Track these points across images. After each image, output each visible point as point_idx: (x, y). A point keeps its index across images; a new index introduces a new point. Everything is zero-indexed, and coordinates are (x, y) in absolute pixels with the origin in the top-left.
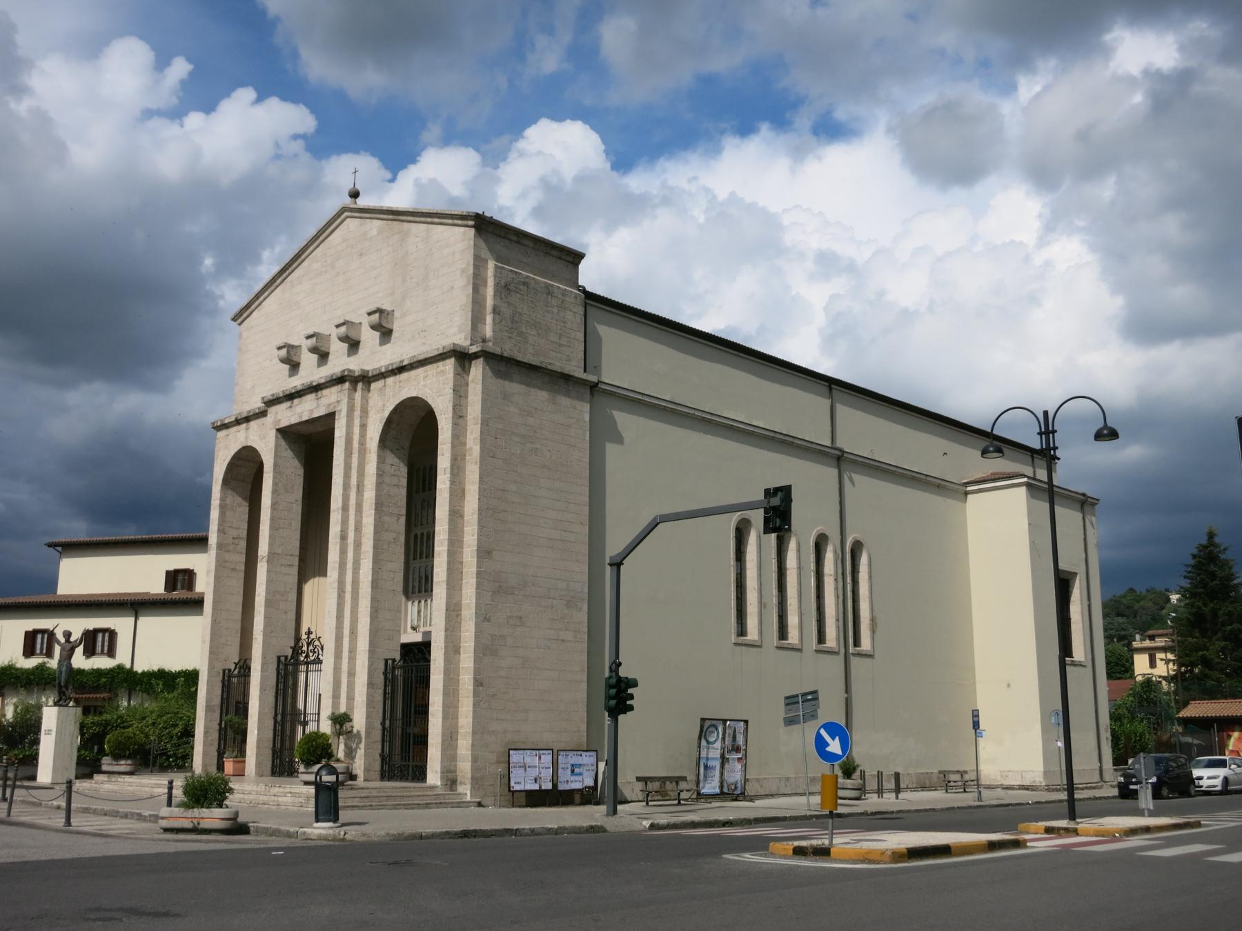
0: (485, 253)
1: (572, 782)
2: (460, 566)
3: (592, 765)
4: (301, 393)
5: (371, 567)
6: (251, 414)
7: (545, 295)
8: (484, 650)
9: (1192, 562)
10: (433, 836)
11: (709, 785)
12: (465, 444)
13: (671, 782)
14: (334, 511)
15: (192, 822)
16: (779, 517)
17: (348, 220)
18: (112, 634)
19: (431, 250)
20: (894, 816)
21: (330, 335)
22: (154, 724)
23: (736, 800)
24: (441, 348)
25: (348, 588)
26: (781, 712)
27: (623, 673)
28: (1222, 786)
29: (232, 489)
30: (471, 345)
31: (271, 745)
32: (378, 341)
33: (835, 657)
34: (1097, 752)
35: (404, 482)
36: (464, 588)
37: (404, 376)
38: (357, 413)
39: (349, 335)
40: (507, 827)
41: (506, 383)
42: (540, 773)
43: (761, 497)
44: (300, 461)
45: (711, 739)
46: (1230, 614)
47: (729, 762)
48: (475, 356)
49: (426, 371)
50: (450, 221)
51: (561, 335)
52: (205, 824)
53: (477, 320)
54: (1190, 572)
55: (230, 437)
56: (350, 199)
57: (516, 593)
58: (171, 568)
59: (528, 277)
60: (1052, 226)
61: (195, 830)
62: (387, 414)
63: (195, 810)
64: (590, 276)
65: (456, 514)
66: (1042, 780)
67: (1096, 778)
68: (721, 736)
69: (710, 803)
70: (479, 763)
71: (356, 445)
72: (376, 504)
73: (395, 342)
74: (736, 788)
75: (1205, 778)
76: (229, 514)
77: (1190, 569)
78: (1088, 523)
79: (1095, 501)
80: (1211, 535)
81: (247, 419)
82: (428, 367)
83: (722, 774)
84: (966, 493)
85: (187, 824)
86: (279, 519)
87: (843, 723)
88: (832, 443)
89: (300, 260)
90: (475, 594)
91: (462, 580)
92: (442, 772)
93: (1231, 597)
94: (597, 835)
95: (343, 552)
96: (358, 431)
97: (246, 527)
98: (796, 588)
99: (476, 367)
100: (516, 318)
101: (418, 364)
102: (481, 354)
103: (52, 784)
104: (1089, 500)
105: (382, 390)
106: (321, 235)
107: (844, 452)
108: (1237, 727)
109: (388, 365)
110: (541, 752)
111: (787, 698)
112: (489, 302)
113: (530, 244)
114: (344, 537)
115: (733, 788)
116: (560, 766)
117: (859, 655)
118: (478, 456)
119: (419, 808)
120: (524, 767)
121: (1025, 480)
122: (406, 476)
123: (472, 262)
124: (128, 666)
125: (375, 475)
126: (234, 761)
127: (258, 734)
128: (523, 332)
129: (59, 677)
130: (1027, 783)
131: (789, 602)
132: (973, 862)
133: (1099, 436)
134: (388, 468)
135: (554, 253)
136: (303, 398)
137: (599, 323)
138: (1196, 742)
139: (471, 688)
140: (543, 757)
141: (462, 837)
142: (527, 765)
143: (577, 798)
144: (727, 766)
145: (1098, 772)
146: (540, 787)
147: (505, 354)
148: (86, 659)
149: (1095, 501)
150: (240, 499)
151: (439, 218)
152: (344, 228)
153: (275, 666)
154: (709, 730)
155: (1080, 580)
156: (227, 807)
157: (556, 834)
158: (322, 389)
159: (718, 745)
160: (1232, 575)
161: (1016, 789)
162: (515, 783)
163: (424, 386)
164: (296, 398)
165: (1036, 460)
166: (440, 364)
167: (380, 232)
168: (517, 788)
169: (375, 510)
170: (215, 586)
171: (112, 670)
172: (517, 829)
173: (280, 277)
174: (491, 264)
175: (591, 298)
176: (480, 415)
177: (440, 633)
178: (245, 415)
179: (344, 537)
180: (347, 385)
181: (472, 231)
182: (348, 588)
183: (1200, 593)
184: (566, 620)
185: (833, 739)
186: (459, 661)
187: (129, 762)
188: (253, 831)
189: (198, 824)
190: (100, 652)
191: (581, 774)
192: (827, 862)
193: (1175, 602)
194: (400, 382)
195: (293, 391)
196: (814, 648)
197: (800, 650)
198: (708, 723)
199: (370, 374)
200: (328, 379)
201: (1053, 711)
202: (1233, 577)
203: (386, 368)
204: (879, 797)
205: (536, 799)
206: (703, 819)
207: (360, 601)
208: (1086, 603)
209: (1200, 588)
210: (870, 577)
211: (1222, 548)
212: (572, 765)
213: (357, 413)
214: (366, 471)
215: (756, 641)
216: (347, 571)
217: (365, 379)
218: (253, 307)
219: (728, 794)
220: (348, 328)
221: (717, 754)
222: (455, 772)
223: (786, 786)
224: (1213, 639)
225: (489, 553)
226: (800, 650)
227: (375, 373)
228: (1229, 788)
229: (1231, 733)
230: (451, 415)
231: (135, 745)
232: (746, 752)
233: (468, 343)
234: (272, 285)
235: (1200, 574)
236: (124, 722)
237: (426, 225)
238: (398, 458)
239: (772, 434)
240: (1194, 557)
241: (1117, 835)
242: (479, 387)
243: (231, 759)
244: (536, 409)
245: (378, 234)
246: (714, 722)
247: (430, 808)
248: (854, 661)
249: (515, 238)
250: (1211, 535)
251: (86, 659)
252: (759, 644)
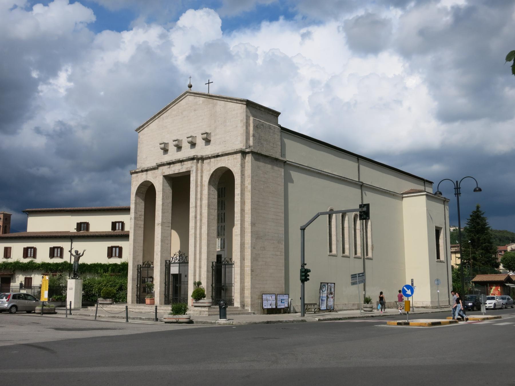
0: (249, 114)
1: (281, 305)
2: (244, 229)
3: (287, 299)
4: (174, 163)
5: (207, 228)
6: (149, 169)
7: (269, 129)
8: (254, 259)
9: (470, 218)
10: (259, 323)
11: (323, 306)
12: (245, 185)
13: (310, 305)
14: (191, 208)
15: (176, 320)
16: (365, 214)
17: (188, 96)
18: (62, 249)
19: (227, 111)
20: (389, 316)
21: (182, 140)
22: (105, 285)
23: (330, 312)
24: (236, 149)
25: (198, 236)
26: (349, 280)
27: (306, 267)
28: (494, 307)
29: (139, 196)
30: (246, 149)
31: (164, 293)
32: (204, 144)
33: (360, 259)
34: (448, 294)
35: (216, 197)
36: (245, 237)
37: (219, 158)
38: (199, 171)
39: (193, 141)
40: (279, 320)
41: (258, 162)
42: (272, 302)
43: (358, 207)
44: (171, 187)
45: (324, 290)
46: (485, 239)
47: (329, 298)
48: (248, 153)
49: (229, 157)
50: (235, 101)
51: (274, 143)
52: (181, 320)
53: (247, 139)
54: (469, 222)
55: (138, 177)
56: (188, 88)
57: (263, 238)
58: (79, 222)
59: (263, 122)
60: (411, 71)
61: (177, 322)
62: (211, 172)
63: (177, 315)
64: (282, 121)
65: (242, 210)
66: (430, 304)
67: (448, 304)
68: (327, 289)
69: (325, 313)
70: (253, 299)
71: (199, 183)
72: (208, 205)
73: (212, 145)
74: (331, 307)
75: (488, 304)
76: (138, 206)
77: (469, 221)
78: (446, 209)
79: (449, 200)
80: (478, 207)
81: (147, 171)
82: (230, 156)
83: (327, 302)
84: (403, 197)
85: (174, 320)
86: (165, 209)
87: (411, 285)
88: (359, 180)
89: (166, 110)
90: (250, 239)
91: (245, 234)
92: (240, 302)
93: (485, 232)
94: (303, 323)
95: (196, 223)
96: (200, 178)
97: (144, 211)
98: (348, 235)
99: (248, 157)
100: (260, 138)
101: (225, 155)
102: (250, 152)
103: (74, 308)
104: (447, 200)
105: (209, 164)
106: (176, 101)
107: (363, 183)
108: (494, 285)
109: (212, 154)
110: (272, 295)
111: (352, 275)
112: (251, 132)
113: (263, 110)
114: (196, 217)
115: (330, 307)
116: (278, 300)
117: (368, 259)
118: (250, 189)
119: (237, 315)
120: (267, 300)
121: (426, 193)
122: (217, 195)
123: (245, 118)
124: (69, 262)
125: (207, 195)
126: (150, 299)
127: (160, 289)
128: (262, 143)
129: (74, 268)
130: (424, 306)
131: (345, 240)
132: (447, 327)
133: (475, 190)
134: (211, 192)
135: (271, 113)
136: (175, 165)
137: (285, 138)
138: (480, 291)
139: (250, 272)
140: (272, 296)
141: (266, 323)
142: (268, 300)
143: (282, 311)
144: (328, 300)
145: (448, 301)
146: (272, 307)
147: (258, 152)
148: (50, 259)
149: (449, 200)
150: (141, 200)
151: (230, 100)
152: (186, 99)
153: (165, 264)
154: (323, 287)
155: (443, 230)
156: (187, 314)
157: (292, 322)
158: (184, 162)
159: (326, 292)
160: (486, 223)
161: (420, 308)
162: (264, 306)
163: (228, 163)
164: (172, 164)
165: (425, 184)
166: (235, 155)
167: (203, 102)
168: (265, 307)
169: (208, 207)
170: (134, 233)
171: (62, 264)
172: (282, 321)
173: (157, 116)
174: (252, 118)
175: (283, 129)
176: (251, 175)
177: (238, 253)
178: (146, 169)
179: (196, 217)
180: (195, 161)
181: (245, 106)
182: (198, 236)
183: (473, 231)
184: (278, 248)
185: (408, 290)
186: (245, 263)
187: (111, 300)
188: (195, 322)
189: (178, 320)
190: (56, 256)
191: (284, 303)
192: (409, 326)
193: (452, 231)
194: (217, 161)
195: (171, 162)
196: (354, 257)
197: (349, 257)
198: (323, 284)
199: (204, 157)
200: (187, 158)
201: (436, 280)
202: (486, 224)
203: (211, 155)
204: (377, 311)
205: (270, 311)
206: (333, 318)
207: (202, 241)
208: (445, 239)
209: (473, 229)
210: (371, 230)
211: (482, 213)
212: (281, 300)
213: (199, 171)
214: (203, 193)
215: (335, 254)
216: (197, 230)
217: (202, 159)
218: (145, 126)
219: (330, 310)
220: (192, 139)
221: (326, 295)
222: (244, 302)
223: (345, 307)
224: (478, 249)
225: (254, 224)
226: (349, 257)
227: (206, 157)
228: (496, 307)
229: (492, 287)
230: (240, 174)
231: (113, 293)
232: (334, 295)
233: (244, 148)
234: (154, 118)
235: (473, 223)
236: (90, 285)
237: (224, 102)
238: (214, 188)
239: (340, 178)
240: (471, 216)
241: (480, 320)
242: (250, 164)
243: (149, 298)
244: (268, 172)
245: (203, 103)
246: (325, 284)
247: (240, 315)
248: (366, 261)
249: (258, 108)
250: (478, 207)
251: (50, 259)
252: (336, 255)
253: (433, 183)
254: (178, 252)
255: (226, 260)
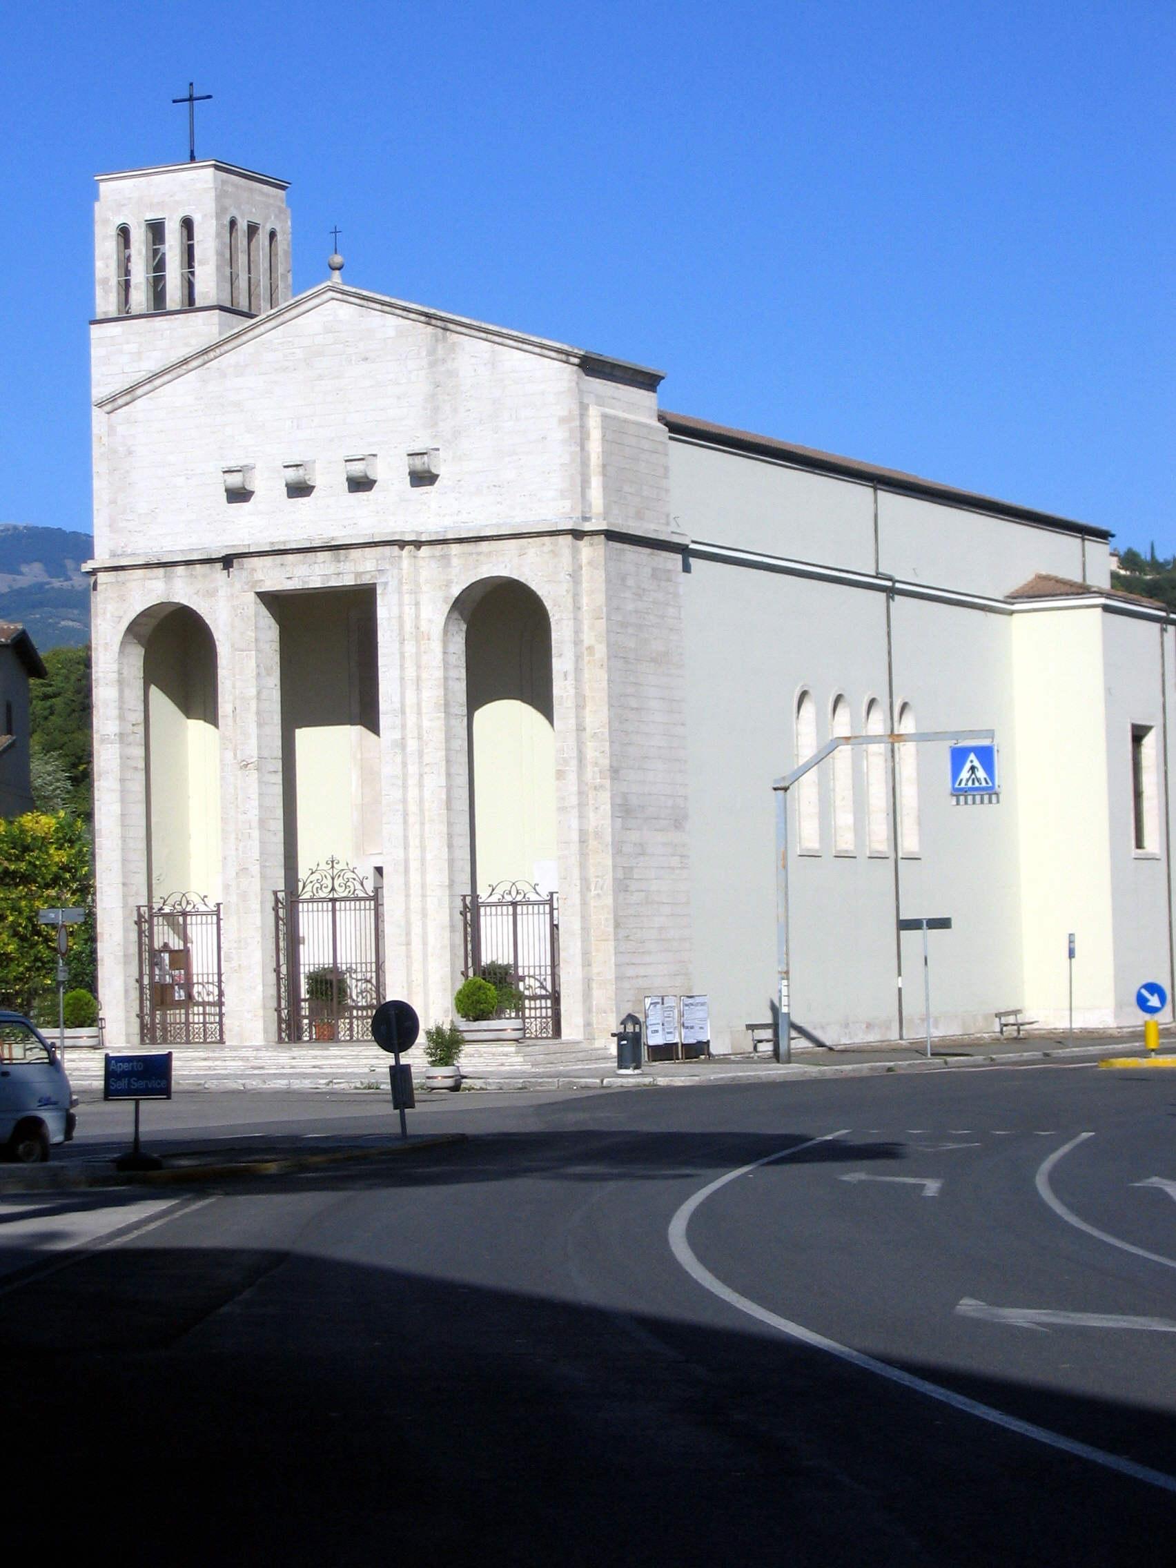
50: (537, 350)
253: (1113, 536)
254: (327, 863)
255: (517, 891)
